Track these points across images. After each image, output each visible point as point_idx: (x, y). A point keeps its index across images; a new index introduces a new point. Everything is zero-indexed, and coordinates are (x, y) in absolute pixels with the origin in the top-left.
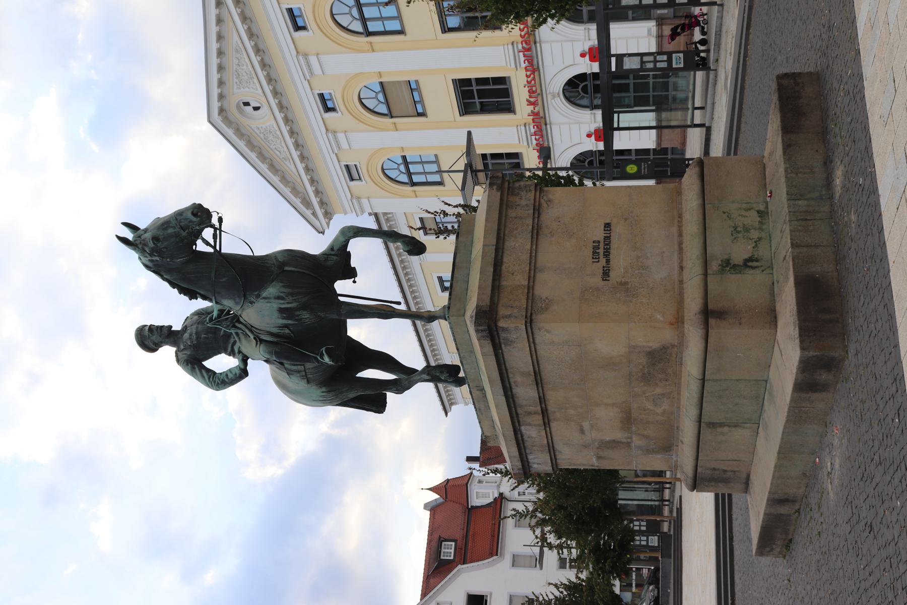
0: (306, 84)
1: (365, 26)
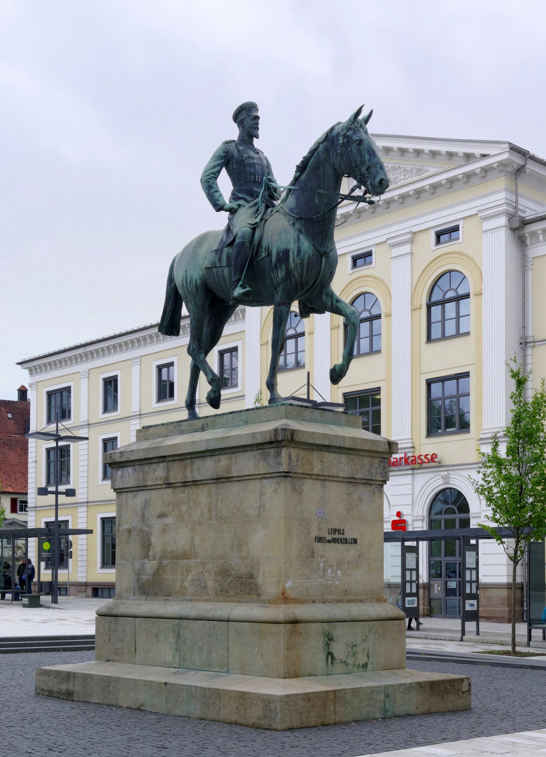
0: (383, 239)
1: (436, 304)
